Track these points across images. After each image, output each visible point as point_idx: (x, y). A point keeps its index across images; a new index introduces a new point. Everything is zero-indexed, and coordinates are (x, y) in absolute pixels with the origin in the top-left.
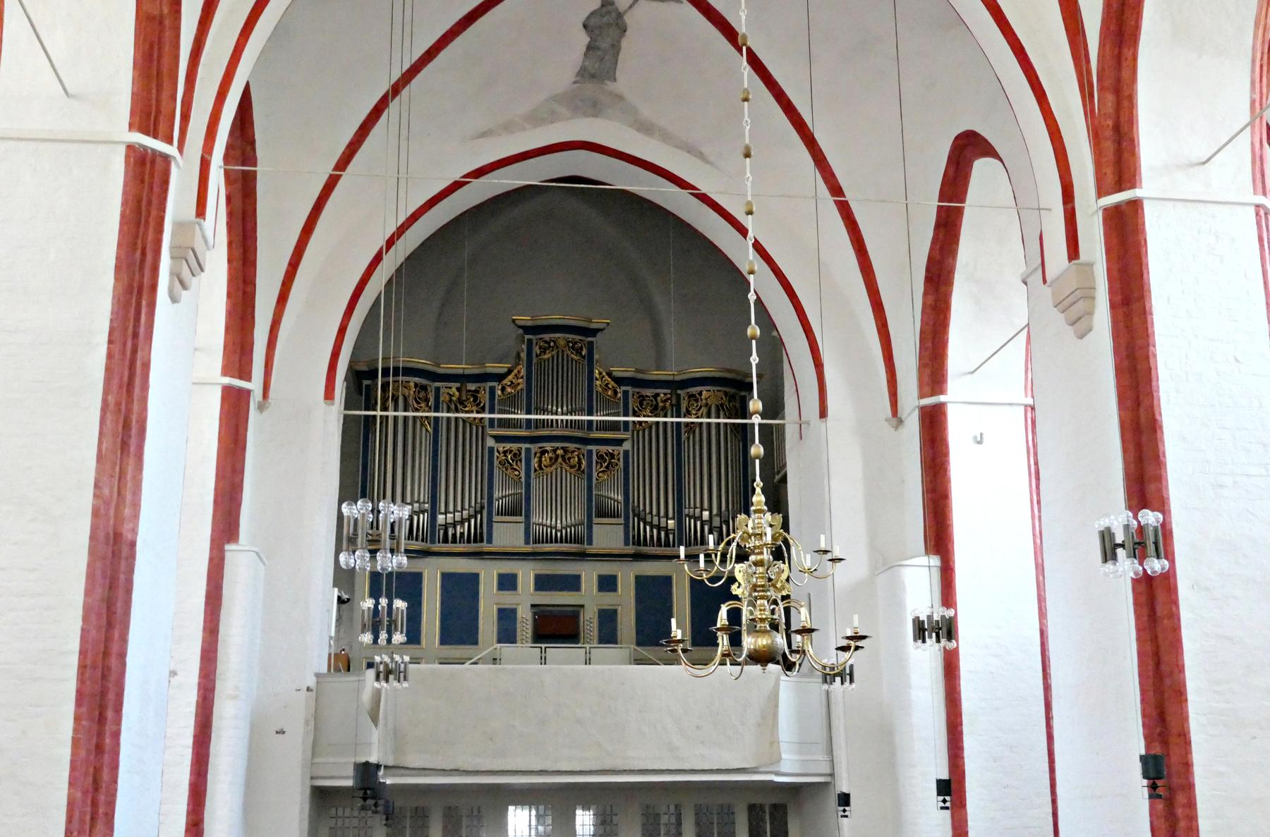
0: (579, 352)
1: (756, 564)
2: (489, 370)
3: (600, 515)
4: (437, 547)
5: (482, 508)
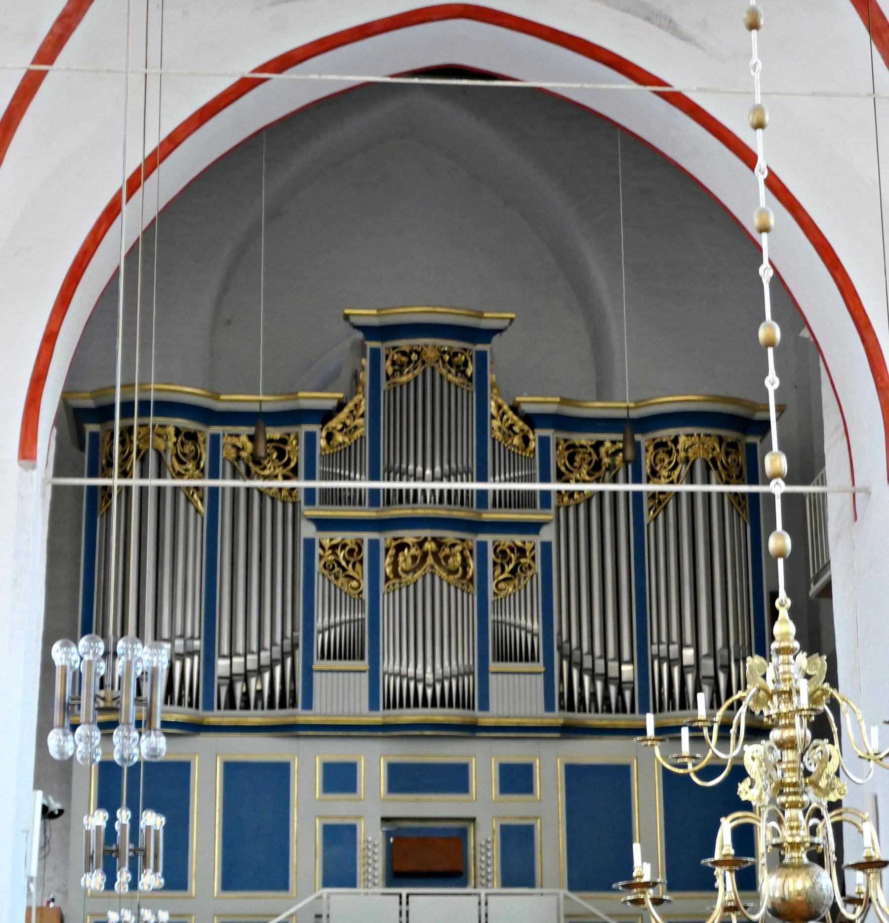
0: (461, 369)
1: (782, 745)
2: (305, 404)
3: (503, 656)
4: (217, 717)
5: (294, 646)
